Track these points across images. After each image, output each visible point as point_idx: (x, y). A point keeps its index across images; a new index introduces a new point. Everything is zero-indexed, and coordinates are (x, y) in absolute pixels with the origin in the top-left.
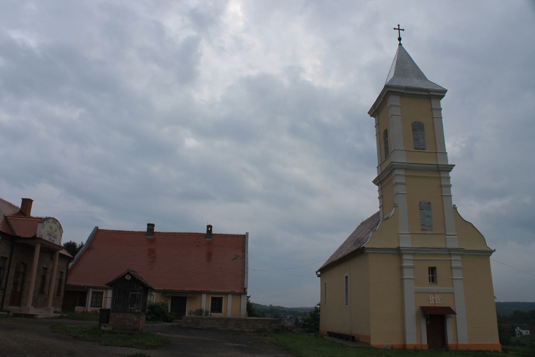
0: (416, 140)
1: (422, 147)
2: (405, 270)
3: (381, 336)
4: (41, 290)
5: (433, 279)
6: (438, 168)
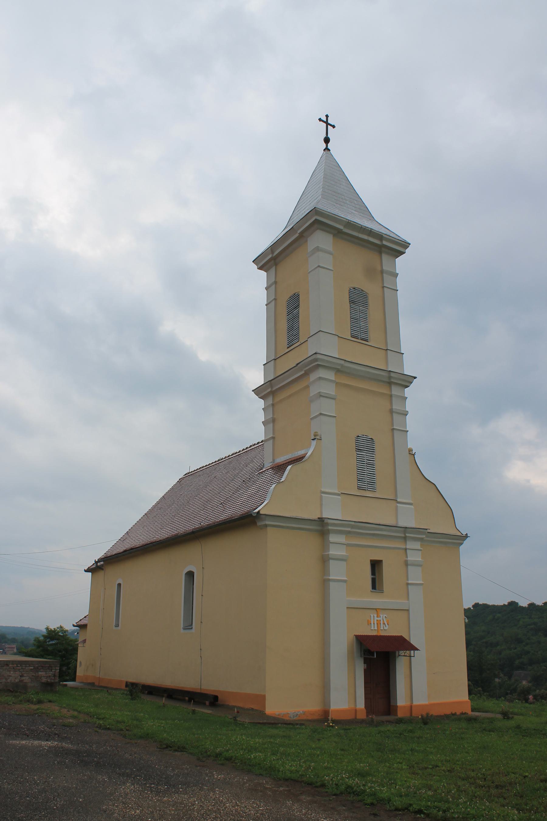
0: (354, 320)
1: (363, 336)
3: (286, 698)
6: (390, 377)
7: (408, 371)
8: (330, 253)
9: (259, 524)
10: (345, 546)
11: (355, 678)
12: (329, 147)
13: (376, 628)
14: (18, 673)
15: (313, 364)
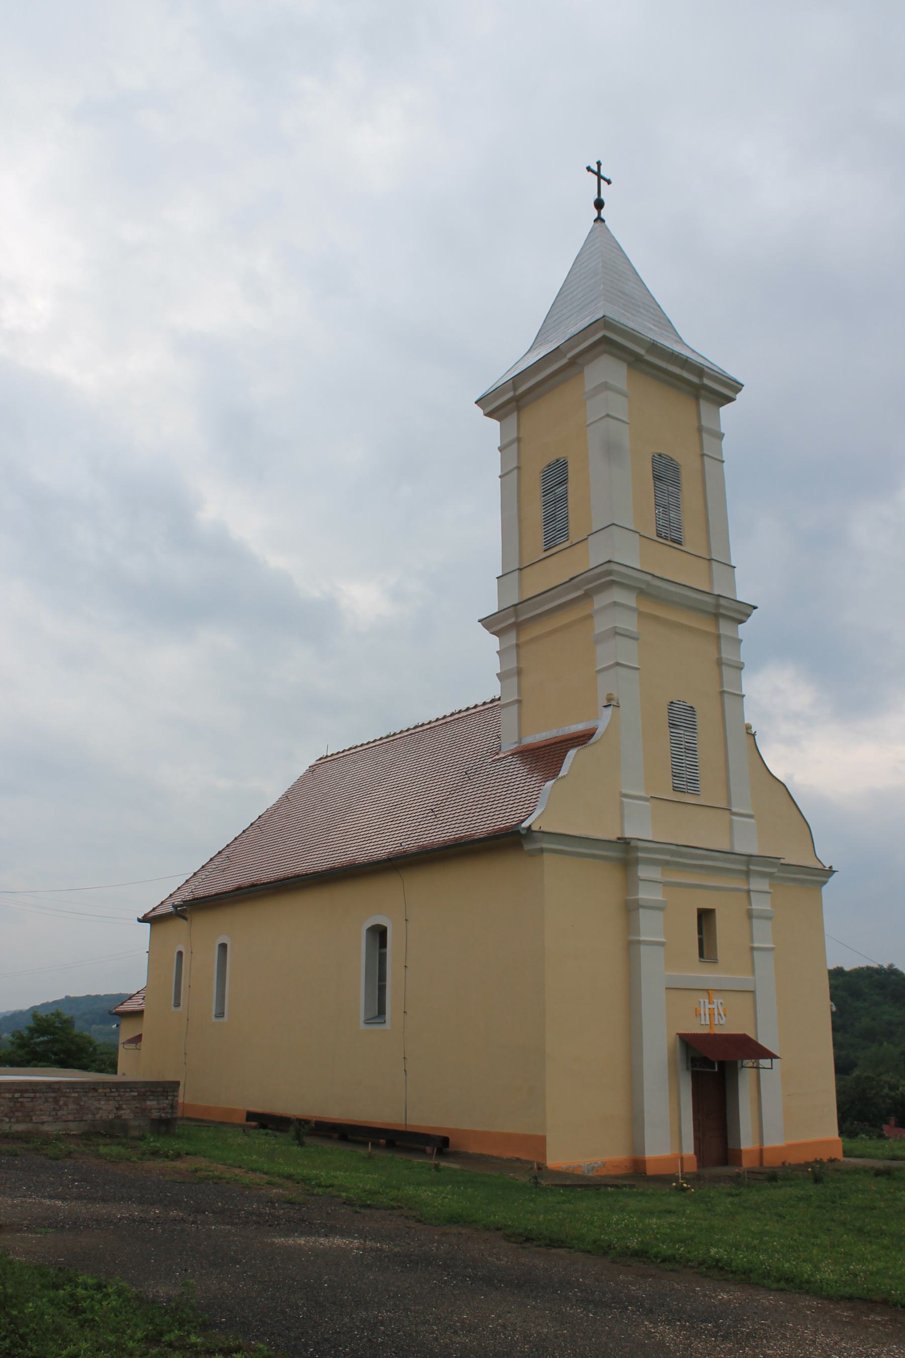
1: (675, 535)
2: (645, 917)
3: (578, 1143)
4: (719, 1014)
5: (706, 949)
6: (718, 606)
7: (743, 595)
8: (626, 396)
9: (527, 847)
10: (661, 885)
11: (679, 1104)
12: (603, 216)
13: (708, 1022)
14: (113, 1104)
15: (605, 579)
